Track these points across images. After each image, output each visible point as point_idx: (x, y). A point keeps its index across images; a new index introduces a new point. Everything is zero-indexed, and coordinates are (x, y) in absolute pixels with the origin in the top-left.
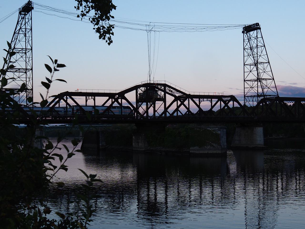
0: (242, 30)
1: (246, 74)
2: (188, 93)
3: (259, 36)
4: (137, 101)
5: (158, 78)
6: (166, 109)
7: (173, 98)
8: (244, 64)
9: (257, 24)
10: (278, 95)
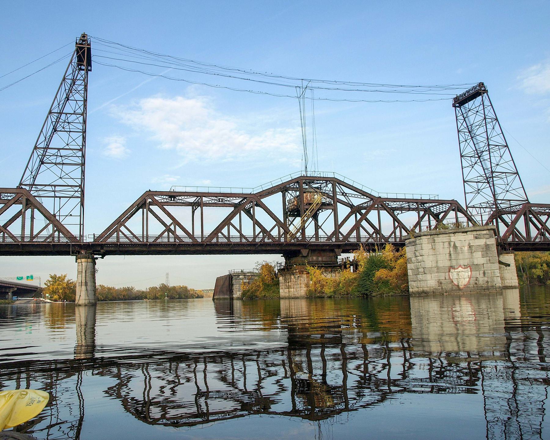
0: (452, 102)
1: (466, 171)
2: (376, 195)
3: (487, 103)
4: (286, 215)
5: (321, 168)
6: (338, 226)
7: (349, 210)
8: (461, 154)
9: (481, 85)
10: (527, 200)
